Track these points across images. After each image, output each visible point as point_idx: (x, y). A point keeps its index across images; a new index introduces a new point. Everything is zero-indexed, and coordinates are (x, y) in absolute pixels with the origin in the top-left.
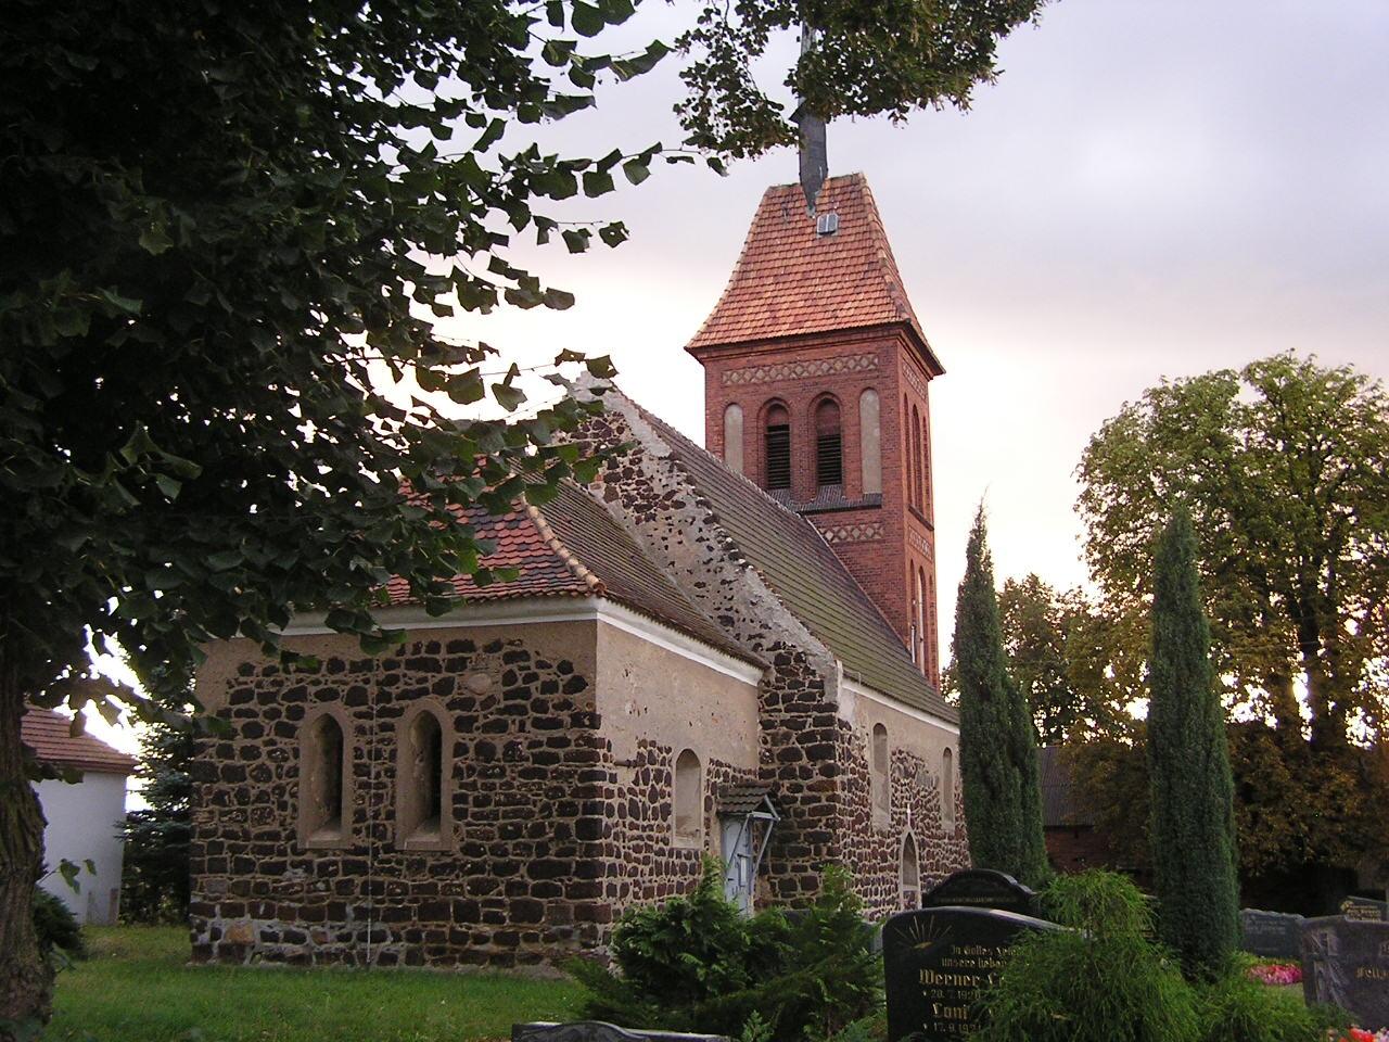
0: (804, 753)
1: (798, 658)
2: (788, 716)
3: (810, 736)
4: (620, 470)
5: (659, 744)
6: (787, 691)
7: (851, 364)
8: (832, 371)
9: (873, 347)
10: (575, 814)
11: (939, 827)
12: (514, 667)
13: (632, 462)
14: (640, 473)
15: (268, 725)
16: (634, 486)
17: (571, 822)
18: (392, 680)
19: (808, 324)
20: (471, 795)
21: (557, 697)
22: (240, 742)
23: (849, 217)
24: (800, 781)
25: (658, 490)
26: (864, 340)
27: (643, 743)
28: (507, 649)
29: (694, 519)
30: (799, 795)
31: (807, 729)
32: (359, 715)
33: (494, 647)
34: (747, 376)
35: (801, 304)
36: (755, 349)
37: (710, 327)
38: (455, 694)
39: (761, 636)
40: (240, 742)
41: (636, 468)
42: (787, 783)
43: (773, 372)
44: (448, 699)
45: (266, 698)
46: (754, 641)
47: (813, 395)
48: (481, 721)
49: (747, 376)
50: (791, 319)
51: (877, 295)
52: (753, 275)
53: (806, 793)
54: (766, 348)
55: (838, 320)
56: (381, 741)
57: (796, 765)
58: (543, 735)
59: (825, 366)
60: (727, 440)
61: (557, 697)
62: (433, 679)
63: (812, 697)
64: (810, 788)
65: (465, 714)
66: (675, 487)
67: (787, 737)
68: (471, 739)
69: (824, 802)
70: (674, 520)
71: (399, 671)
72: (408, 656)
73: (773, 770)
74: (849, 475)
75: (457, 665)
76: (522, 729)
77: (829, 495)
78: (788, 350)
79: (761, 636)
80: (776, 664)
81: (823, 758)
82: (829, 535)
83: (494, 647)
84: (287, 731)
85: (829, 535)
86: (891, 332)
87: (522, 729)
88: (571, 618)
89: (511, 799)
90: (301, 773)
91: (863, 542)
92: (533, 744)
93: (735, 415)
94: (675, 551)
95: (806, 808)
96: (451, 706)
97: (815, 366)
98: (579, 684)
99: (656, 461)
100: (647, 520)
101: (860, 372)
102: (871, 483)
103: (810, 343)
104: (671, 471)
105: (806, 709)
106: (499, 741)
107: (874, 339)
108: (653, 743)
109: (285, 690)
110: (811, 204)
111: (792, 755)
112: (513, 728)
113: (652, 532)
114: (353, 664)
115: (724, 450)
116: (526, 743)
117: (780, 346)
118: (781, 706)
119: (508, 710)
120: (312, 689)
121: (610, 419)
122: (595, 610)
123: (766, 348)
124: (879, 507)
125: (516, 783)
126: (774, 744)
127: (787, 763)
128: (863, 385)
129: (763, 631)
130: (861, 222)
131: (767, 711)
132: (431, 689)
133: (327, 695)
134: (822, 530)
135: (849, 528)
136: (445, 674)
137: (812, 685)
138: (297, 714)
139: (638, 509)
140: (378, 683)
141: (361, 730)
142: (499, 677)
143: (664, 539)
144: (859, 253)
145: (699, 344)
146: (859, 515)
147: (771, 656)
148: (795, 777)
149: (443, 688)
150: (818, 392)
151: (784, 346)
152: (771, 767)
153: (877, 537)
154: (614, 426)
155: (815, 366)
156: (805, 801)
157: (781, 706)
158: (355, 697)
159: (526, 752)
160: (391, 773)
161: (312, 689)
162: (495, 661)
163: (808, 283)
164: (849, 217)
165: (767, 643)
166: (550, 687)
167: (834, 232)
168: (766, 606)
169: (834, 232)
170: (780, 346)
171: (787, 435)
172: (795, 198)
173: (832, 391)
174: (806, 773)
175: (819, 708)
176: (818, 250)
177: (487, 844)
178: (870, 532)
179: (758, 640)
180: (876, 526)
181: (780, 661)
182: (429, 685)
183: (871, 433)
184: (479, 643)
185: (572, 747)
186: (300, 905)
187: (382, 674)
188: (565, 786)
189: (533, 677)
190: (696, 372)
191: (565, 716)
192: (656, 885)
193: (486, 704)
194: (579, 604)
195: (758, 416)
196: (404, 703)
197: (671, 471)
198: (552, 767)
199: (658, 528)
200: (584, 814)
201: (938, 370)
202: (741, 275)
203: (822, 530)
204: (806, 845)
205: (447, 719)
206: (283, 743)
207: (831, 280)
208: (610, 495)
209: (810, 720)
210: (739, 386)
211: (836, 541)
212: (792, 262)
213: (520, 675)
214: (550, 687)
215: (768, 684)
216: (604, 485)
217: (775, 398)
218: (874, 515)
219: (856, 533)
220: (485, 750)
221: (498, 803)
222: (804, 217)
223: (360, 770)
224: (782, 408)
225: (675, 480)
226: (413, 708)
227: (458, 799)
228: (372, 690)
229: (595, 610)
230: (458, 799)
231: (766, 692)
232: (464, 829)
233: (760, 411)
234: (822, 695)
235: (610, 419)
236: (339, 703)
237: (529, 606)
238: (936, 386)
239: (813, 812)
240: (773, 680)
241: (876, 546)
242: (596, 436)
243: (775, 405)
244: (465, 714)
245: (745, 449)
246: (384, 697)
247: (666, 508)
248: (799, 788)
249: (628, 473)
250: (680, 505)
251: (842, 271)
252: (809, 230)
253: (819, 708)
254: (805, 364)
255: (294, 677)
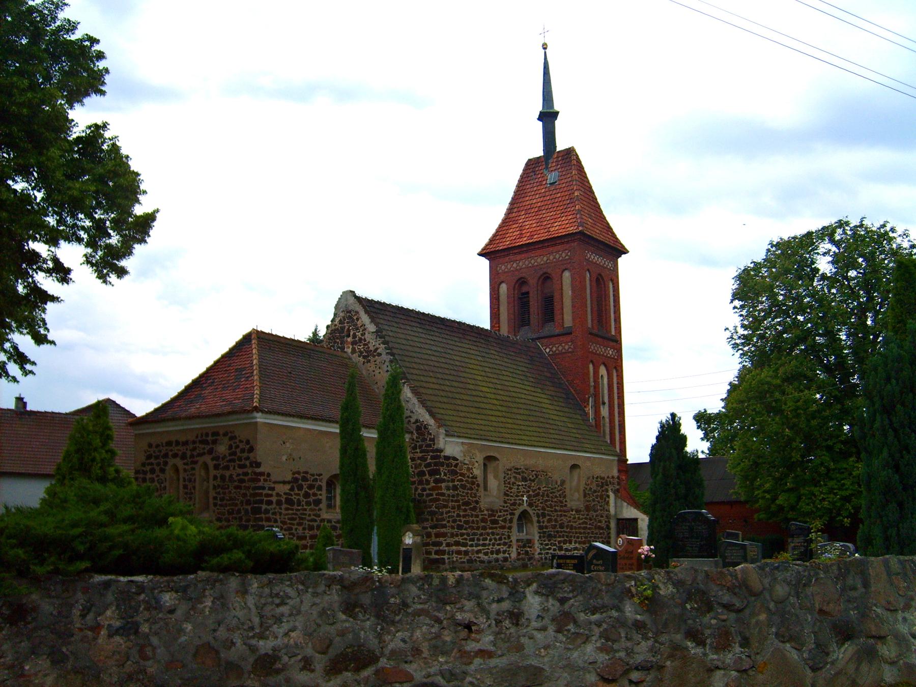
0: (427, 473)
1: (425, 428)
2: (421, 455)
3: (429, 465)
4: (357, 339)
5: (311, 472)
6: (420, 443)
7: (557, 256)
8: (548, 261)
9: (567, 246)
10: (250, 504)
11: (566, 505)
12: (232, 442)
13: (362, 335)
14: (365, 340)
15: (157, 468)
16: (362, 347)
17: (249, 508)
18: (194, 449)
19: (535, 236)
20: (219, 497)
21: (245, 455)
22: (149, 476)
23: (564, 173)
24: (425, 486)
25: (372, 348)
26: (563, 243)
27: (294, 474)
28: (230, 435)
29: (385, 361)
30: (425, 493)
31: (428, 461)
32: (184, 464)
33: (225, 435)
34: (509, 267)
35: (535, 225)
36: (511, 252)
37: (491, 241)
38: (214, 455)
39: (410, 417)
40: (149, 476)
41: (363, 338)
42: (420, 487)
43: (521, 264)
44: (211, 456)
45: (157, 457)
46: (408, 419)
47: (539, 275)
48: (222, 466)
49: (509, 267)
50: (528, 234)
51: (571, 217)
52: (515, 210)
53: (428, 492)
54: (516, 251)
55: (550, 233)
56: (191, 474)
57: (424, 478)
58: (240, 471)
59: (545, 259)
60: (500, 302)
61: (245, 455)
62: (207, 447)
63: (430, 446)
64: (429, 489)
65: (217, 462)
66: (378, 346)
67: (420, 465)
68: (218, 473)
69: (435, 496)
70: (377, 362)
71: (197, 445)
72: (199, 438)
73: (415, 481)
74: (557, 317)
75: (215, 442)
76: (234, 469)
77: (549, 329)
78: (527, 251)
79: (410, 417)
80: (416, 431)
81: (434, 475)
82: (548, 350)
83: (225, 435)
84: (163, 471)
85: (548, 350)
86: (576, 238)
87: (234, 469)
88: (248, 421)
89: (231, 499)
90: (167, 489)
91: (564, 353)
92: (238, 475)
93: (504, 288)
94: (378, 376)
95: (428, 499)
96: (213, 459)
97: (540, 260)
98: (251, 450)
99: (371, 333)
100: (367, 362)
101: (561, 261)
102: (568, 321)
103: (537, 247)
104: (376, 338)
105: (428, 452)
106: (227, 474)
107: (568, 242)
108: (307, 473)
109: (162, 454)
110: (547, 168)
111: (422, 473)
112: (231, 468)
113: (369, 368)
114: (183, 442)
115: (499, 307)
116: (235, 474)
117: (523, 250)
118: (418, 450)
119: (230, 461)
120: (170, 453)
121: (353, 314)
122: (256, 418)
123: (516, 251)
124: (571, 333)
125: (232, 492)
126: (415, 469)
127: (420, 478)
128: (563, 267)
129: (411, 414)
130: (569, 176)
131: (412, 453)
132: (180, 455)
133: (175, 456)
134: (544, 348)
135: (557, 346)
136: (211, 446)
137: (430, 439)
138: (166, 463)
139: (364, 357)
140: (190, 450)
141: (185, 470)
142: (227, 447)
143: (374, 371)
144: (566, 193)
145: (484, 252)
146: (561, 339)
147: (414, 426)
148: (423, 484)
149: (211, 452)
150: (542, 273)
151: (525, 249)
152: (414, 479)
153: (570, 350)
154: (355, 318)
155: (540, 260)
156: (428, 495)
157: (418, 450)
158: (183, 457)
159: (236, 478)
160: (194, 488)
161: (170, 453)
162: (226, 440)
163: (540, 213)
164: (564, 173)
165: (413, 420)
166: (243, 451)
167: (556, 182)
168: (412, 402)
169: (556, 182)
170: (523, 250)
171: (528, 297)
172: (540, 164)
173: (549, 272)
174: (428, 482)
175: (433, 451)
176: (547, 194)
177: (224, 517)
178: (567, 347)
179: (409, 419)
180: (570, 344)
181: (418, 429)
182: (206, 451)
183: (568, 292)
184: (221, 433)
185: (250, 476)
186: (626, 573)
187: (191, 446)
188: (247, 492)
189: (237, 447)
190: (485, 263)
191: (248, 463)
192: (308, 535)
193: (223, 459)
194: (251, 416)
195: (514, 287)
196: (198, 458)
197: (376, 338)
198: (244, 484)
199: (371, 367)
200: (254, 504)
201: (623, 251)
202: (510, 211)
203: (544, 348)
204: (427, 517)
205: (211, 464)
206: (162, 475)
207: (551, 210)
208: (354, 351)
209: (429, 457)
210: (505, 273)
211: (551, 353)
212: (534, 201)
213: (234, 445)
214: (243, 451)
215: (413, 440)
216: (351, 347)
217: (521, 278)
218: (569, 338)
219: (560, 348)
220: (223, 478)
221: (227, 500)
222: (542, 175)
223: (185, 487)
224: (525, 282)
225: (378, 342)
226: (201, 460)
227: (215, 498)
228: (189, 454)
229: (256, 418)
230: (215, 498)
231: (412, 443)
232: (216, 511)
233: (515, 285)
234: (434, 445)
235: (353, 314)
236: (178, 459)
237: (235, 417)
238: (622, 261)
239: (431, 501)
240: (415, 438)
241: (570, 355)
242: (348, 323)
243: (522, 282)
244: (217, 462)
245: (508, 306)
246: (192, 456)
247: (374, 356)
248: (424, 490)
249: (360, 339)
250: (380, 355)
251: (557, 204)
252: (544, 182)
253: (433, 451)
254: (536, 258)
255: (164, 448)
